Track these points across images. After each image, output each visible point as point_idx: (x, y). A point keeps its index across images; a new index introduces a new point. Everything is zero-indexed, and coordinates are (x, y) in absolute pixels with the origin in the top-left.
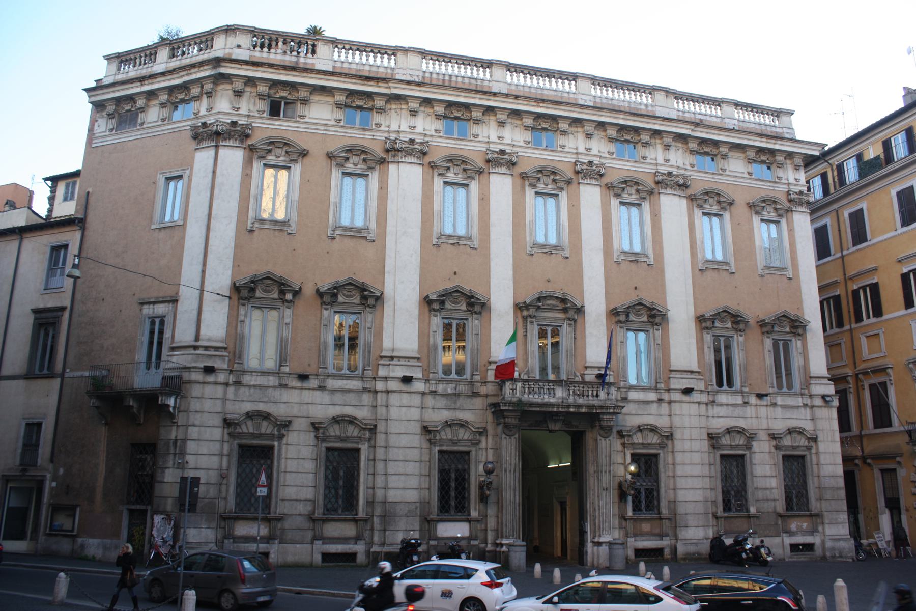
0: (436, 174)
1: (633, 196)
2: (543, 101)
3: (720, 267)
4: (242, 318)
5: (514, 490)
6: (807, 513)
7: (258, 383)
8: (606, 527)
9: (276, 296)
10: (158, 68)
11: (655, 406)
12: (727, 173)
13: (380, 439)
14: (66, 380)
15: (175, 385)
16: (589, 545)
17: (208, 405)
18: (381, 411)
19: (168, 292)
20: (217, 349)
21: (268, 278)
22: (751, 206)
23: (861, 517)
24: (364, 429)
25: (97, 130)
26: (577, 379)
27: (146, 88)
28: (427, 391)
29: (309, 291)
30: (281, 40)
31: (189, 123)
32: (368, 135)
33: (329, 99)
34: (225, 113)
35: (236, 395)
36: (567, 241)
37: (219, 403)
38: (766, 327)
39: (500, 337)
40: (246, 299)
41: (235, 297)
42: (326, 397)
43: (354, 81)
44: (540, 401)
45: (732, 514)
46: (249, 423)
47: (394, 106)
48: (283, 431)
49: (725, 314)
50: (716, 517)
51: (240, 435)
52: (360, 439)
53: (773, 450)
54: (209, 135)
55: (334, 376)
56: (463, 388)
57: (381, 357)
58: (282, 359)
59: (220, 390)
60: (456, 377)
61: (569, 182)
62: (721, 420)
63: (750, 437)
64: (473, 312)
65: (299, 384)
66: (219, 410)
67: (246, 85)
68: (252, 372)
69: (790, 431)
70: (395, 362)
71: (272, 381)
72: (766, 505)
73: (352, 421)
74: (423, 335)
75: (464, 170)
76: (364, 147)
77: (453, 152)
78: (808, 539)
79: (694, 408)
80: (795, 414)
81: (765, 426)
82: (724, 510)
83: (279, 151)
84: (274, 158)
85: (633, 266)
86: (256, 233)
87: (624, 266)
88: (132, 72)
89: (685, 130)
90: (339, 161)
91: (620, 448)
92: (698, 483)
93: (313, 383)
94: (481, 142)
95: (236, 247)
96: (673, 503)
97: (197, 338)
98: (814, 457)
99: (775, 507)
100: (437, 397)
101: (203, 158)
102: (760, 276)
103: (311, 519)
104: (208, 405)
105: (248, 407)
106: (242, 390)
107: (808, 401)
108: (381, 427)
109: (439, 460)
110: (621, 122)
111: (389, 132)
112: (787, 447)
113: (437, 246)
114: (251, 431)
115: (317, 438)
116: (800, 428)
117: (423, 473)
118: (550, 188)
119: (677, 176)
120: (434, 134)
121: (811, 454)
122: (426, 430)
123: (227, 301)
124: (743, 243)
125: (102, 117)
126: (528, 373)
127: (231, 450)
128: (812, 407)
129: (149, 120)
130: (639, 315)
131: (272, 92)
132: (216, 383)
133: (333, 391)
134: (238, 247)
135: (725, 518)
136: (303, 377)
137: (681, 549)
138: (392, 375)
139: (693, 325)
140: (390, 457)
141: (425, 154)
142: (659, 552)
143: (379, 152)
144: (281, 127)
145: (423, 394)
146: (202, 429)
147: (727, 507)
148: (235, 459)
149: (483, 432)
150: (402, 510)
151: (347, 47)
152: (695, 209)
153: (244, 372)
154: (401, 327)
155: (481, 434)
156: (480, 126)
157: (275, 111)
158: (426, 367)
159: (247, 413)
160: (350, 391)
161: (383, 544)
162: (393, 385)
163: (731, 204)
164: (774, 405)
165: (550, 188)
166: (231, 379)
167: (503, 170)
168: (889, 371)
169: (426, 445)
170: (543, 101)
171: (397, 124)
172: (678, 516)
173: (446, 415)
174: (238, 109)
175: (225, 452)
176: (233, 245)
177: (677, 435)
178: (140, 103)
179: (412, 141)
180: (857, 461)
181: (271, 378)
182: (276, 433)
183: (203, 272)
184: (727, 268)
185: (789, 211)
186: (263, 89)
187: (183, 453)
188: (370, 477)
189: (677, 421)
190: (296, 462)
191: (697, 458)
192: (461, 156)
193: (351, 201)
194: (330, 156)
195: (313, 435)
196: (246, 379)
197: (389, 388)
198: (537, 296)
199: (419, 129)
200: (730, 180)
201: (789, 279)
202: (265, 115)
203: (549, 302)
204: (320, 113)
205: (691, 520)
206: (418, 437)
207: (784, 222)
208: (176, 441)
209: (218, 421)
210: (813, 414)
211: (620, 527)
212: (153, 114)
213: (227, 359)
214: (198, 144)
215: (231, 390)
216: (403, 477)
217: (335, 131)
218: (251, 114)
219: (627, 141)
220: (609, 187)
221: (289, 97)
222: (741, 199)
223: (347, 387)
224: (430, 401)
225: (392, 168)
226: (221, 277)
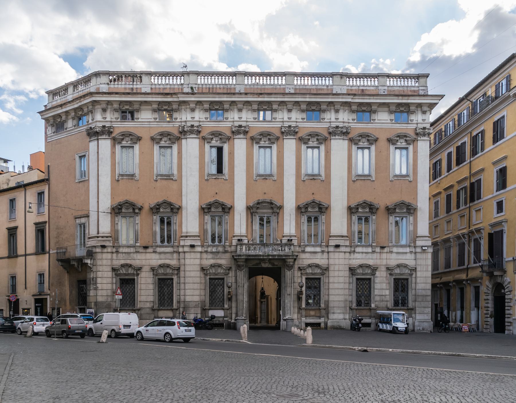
0: (206, 142)
1: (315, 143)
2: (261, 94)
3: (366, 178)
4: (137, 222)
5: (243, 295)
6: (406, 308)
7: (126, 251)
9: (131, 211)
10: (70, 98)
11: (320, 254)
12: (376, 121)
13: (182, 274)
14: (51, 255)
15: (90, 254)
16: (282, 320)
17: (105, 262)
18: (182, 261)
19: (86, 212)
20: (107, 237)
21: (127, 203)
22: (390, 141)
23: (464, 312)
24: (175, 269)
25: (48, 133)
26: (278, 242)
27: (64, 110)
28: (203, 251)
29: (146, 207)
30: (123, 76)
31: (85, 127)
32: (370, 126)
33: (150, 107)
34: (99, 121)
35: (117, 257)
36: (276, 171)
37: (109, 261)
39: (240, 224)
40: (117, 213)
41: (113, 213)
42: (156, 256)
43: (160, 96)
44: (254, 254)
45: (361, 308)
46: (123, 269)
47: (183, 107)
48: (138, 272)
49: (365, 204)
50: (351, 309)
51: (120, 275)
52: (172, 274)
53: (388, 276)
54: (93, 134)
55: (160, 247)
56: (221, 249)
58: (136, 240)
59: (109, 256)
60: (218, 244)
61: (278, 139)
62: (357, 259)
63: (374, 270)
64: (225, 212)
65: (144, 251)
66: (110, 264)
68: (123, 246)
69: (399, 266)
70: (188, 238)
71: (132, 250)
72: (381, 303)
73: (168, 266)
74: (202, 224)
75: (220, 138)
76: (168, 132)
77: (215, 129)
79: (342, 255)
81: (384, 262)
82: (357, 306)
83: (127, 138)
84: (125, 142)
86: (120, 182)
87: (307, 182)
88: (58, 100)
89: (349, 99)
90: (157, 141)
91: (299, 275)
92: (341, 292)
93: (150, 250)
94: (230, 122)
95: (112, 189)
96: (327, 302)
97: (98, 233)
98: (414, 280)
99: (387, 305)
100: (208, 254)
101: (93, 145)
102: (391, 181)
103: (153, 310)
104: (105, 262)
105: (123, 262)
106: (119, 255)
108: (182, 268)
109: (209, 282)
110: (308, 100)
111: (181, 122)
113: (207, 180)
114: (124, 272)
115: (153, 274)
116: (404, 264)
117: (202, 288)
118: (267, 144)
119: (342, 128)
120: (204, 120)
121: (411, 278)
122: (203, 269)
123: (110, 215)
124: (382, 164)
125: (49, 126)
126: (253, 240)
127: (116, 281)
129: (69, 127)
130: (314, 208)
132: (108, 252)
133: (160, 253)
135: (356, 309)
136: (146, 248)
137: (329, 324)
138: (186, 244)
139: (345, 211)
141: (200, 132)
142: (319, 324)
143: (176, 133)
144: (128, 125)
145: (201, 252)
146: (103, 273)
147: (359, 303)
148: (118, 285)
149: (230, 269)
150: (191, 305)
151: (158, 75)
152: (353, 146)
153: (119, 247)
154: (190, 222)
155: (229, 270)
156: (229, 112)
157: (124, 118)
158: (202, 240)
159: (122, 265)
160: (168, 253)
162: (186, 249)
163: (376, 140)
164: (391, 252)
165: (267, 144)
166: (114, 250)
167: (241, 136)
168: (482, 231)
169: (203, 276)
170: (261, 94)
171: (185, 117)
172: (329, 308)
173: (212, 262)
175: (114, 282)
176: (110, 188)
177: (331, 268)
178: (64, 118)
179: (192, 126)
180: (464, 282)
181: (132, 249)
182: (135, 273)
183: (98, 202)
184: (370, 178)
185: (414, 141)
186: (116, 106)
187: (96, 283)
188: (178, 291)
189: (331, 262)
190: (145, 285)
191: (341, 280)
192: (218, 131)
193: (162, 161)
194: (153, 139)
195: (152, 273)
196: (121, 250)
197: (185, 250)
198: (256, 202)
199: (197, 119)
201: (410, 182)
202: (119, 120)
203: (264, 204)
204: (146, 116)
205: (337, 310)
206: (199, 272)
207: (411, 148)
208: (93, 278)
209: (109, 269)
210: (416, 257)
211: (298, 313)
212: (70, 124)
213: (112, 241)
214: (90, 138)
215: (115, 255)
216: (192, 290)
218: (112, 120)
219: (313, 110)
220: (301, 139)
221: (130, 109)
223: (166, 251)
224: (205, 256)
225: (184, 141)
226: (106, 203)
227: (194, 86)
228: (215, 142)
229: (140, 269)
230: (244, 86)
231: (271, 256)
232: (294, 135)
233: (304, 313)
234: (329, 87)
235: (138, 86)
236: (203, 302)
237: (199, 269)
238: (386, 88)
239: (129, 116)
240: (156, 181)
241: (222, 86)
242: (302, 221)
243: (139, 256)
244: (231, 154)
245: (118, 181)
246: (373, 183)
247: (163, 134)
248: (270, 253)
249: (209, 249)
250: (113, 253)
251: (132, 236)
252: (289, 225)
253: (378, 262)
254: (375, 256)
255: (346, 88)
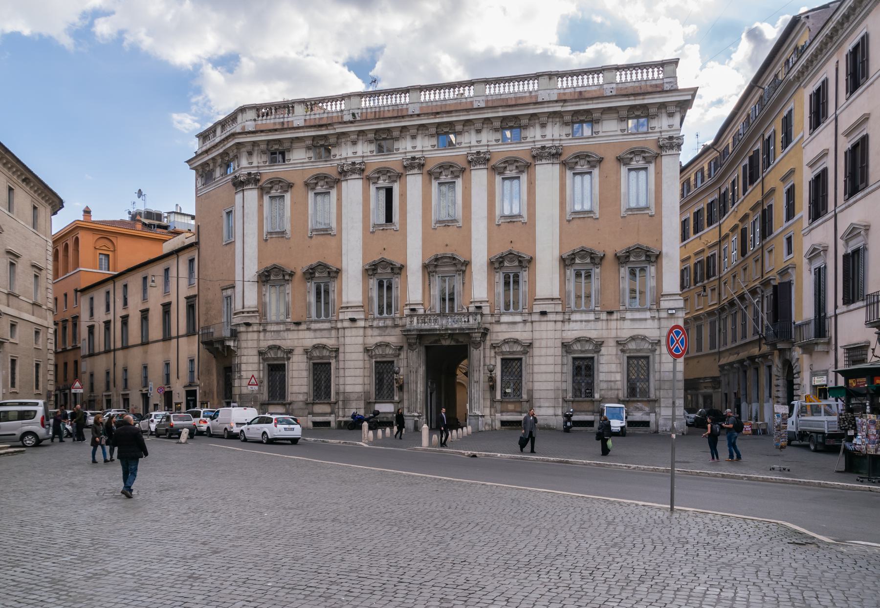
2: (438, 113)
8: (480, 408)
11: (521, 325)
13: (341, 356)
17: (250, 344)
18: (341, 340)
20: (253, 312)
22: (620, 160)
29: (299, 273)
32: (328, 164)
33: (303, 144)
38: (622, 259)
39: (414, 289)
52: (330, 357)
53: (619, 352)
54: (239, 184)
55: (315, 322)
57: (342, 308)
59: (255, 336)
62: (574, 330)
67: (548, 117)
71: (282, 327)
72: (610, 393)
73: (324, 347)
78: (645, 418)
79: (551, 326)
80: (642, 325)
81: (613, 334)
85: (510, 224)
87: (503, 226)
92: (550, 377)
93: (303, 327)
96: (531, 392)
98: (657, 358)
104: (250, 344)
105: (271, 343)
106: (267, 334)
107: (656, 315)
108: (341, 350)
110: (501, 114)
112: (631, 350)
119: (550, 148)
128: (659, 319)
131: (504, 124)
133: (315, 330)
134: (260, 251)
136: (298, 324)
139: (557, 264)
140: (346, 366)
143: (334, 174)
144: (278, 170)
145: (365, 328)
149: (401, 348)
153: (267, 324)
154: (352, 289)
157: (273, 161)
160: (324, 329)
161: (344, 417)
162: (346, 324)
163: (600, 160)
164: (623, 319)
165: (641, 164)
167: (416, 171)
169: (367, 358)
170: (438, 113)
173: (379, 339)
174: (252, 163)
177: (536, 344)
189: (537, 335)
191: (551, 360)
196: (269, 328)
200: (602, 140)
201: (651, 216)
204: (299, 156)
209: (255, 352)
215: (262, 334)
217: (308, 166)
222: (299, 181)
224: (369, 332)
225: (344, 184)
226: (252, 269)
227: (356, 111)
228: (382, 183)
229: (291, 351)
230: (419, 105)
231: (451, 329)
232: (485, 164)
233: (498, 406)
234: (533, 94)
235: (290, 119)
236: (367, 394)
237: (362, 349)
238: (614, 86)
239: (280, 157)
240: (311, 237)
241: (391, 108)
242: (497, 280)
243: (291, 335)
244: (403, 195)
245: (266, 240)
246: (596, 221)
247: (318, 178)
248: (449, 326)
249: (375, 323)
250: (260, 332)
251: (282, 310)
252: (480, 286)
253: (605, 334)
254: (599, 325)
255: (556, 91)
